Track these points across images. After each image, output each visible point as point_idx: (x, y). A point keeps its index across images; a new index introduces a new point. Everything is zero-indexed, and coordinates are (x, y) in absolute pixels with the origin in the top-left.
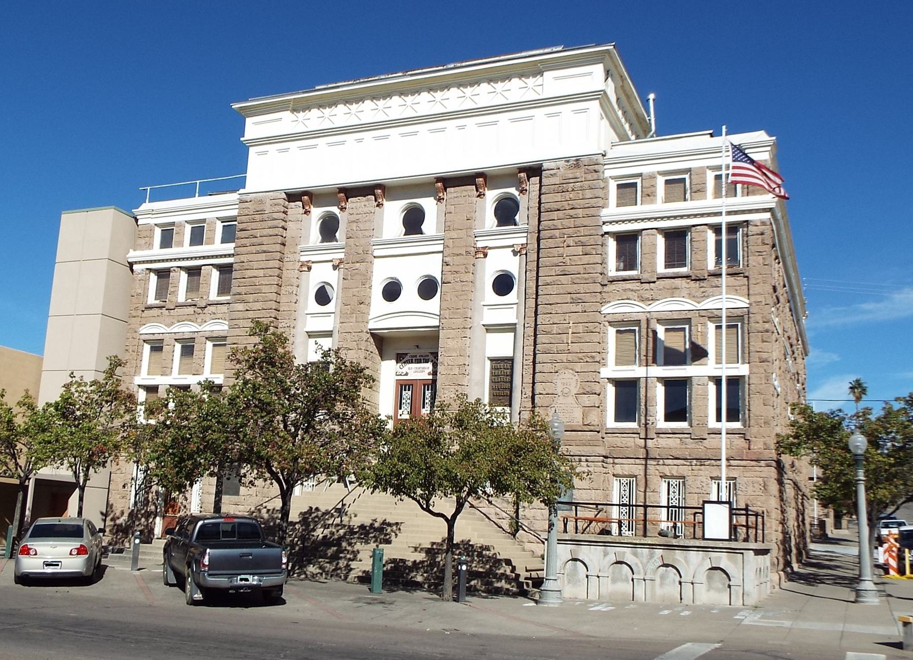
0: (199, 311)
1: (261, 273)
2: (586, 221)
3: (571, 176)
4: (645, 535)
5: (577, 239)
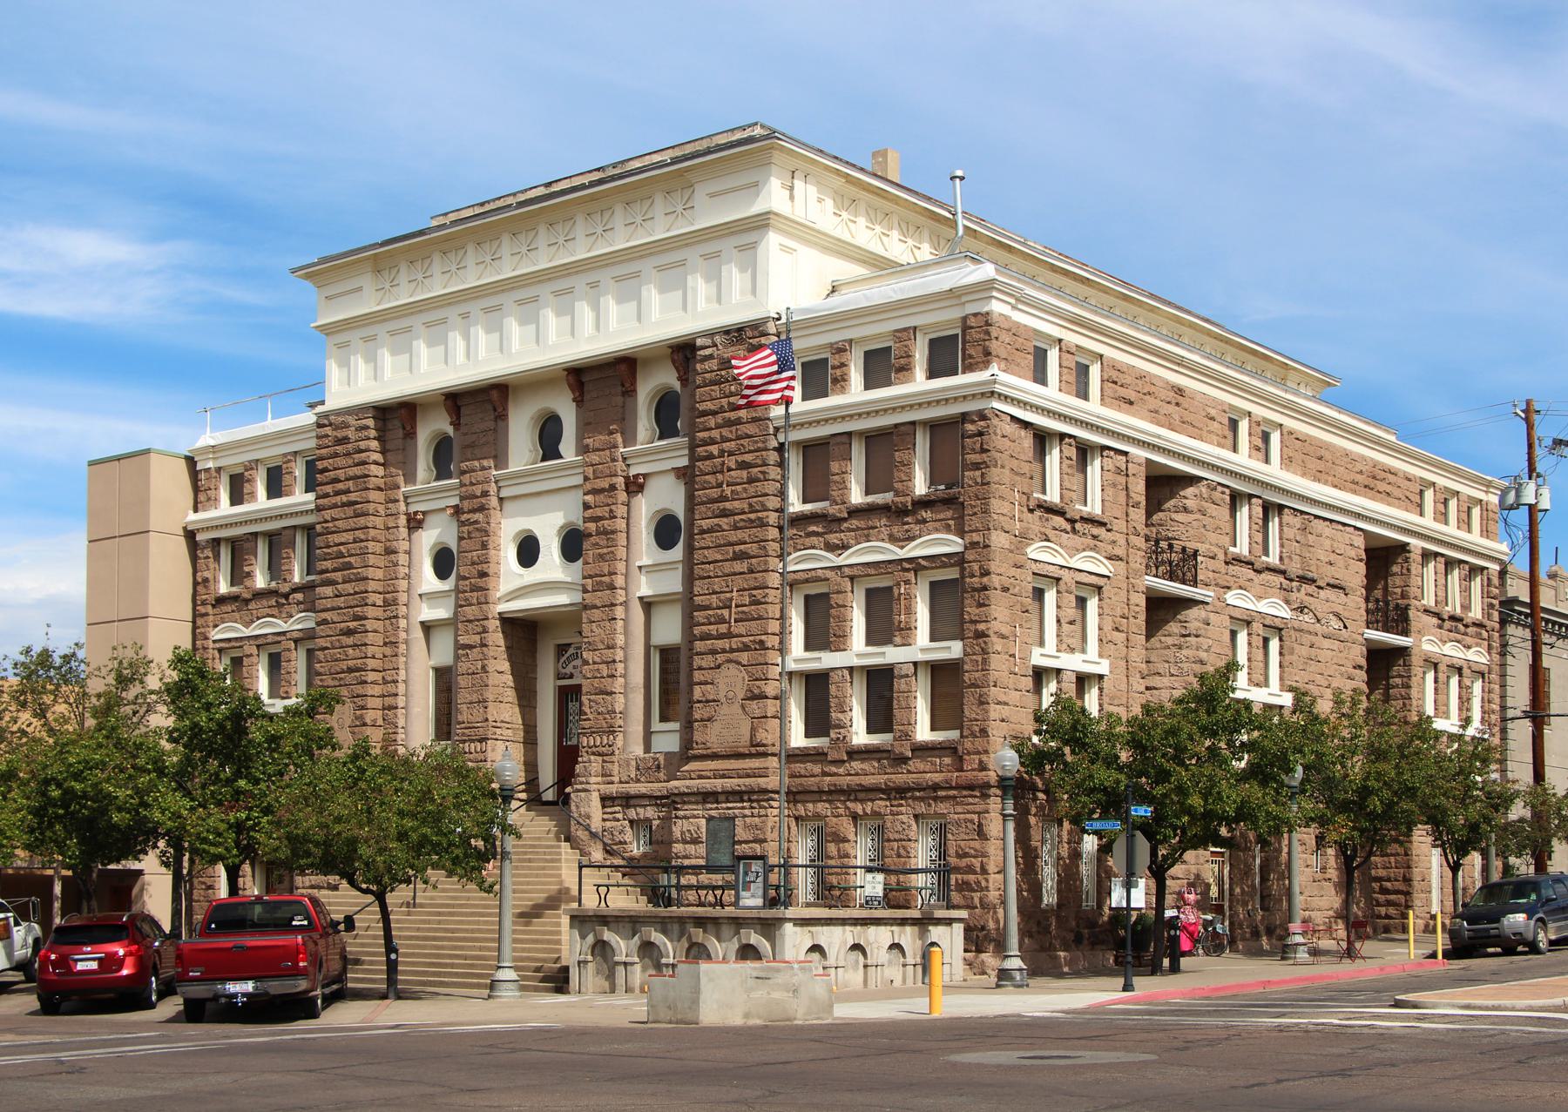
5: (740, 458)
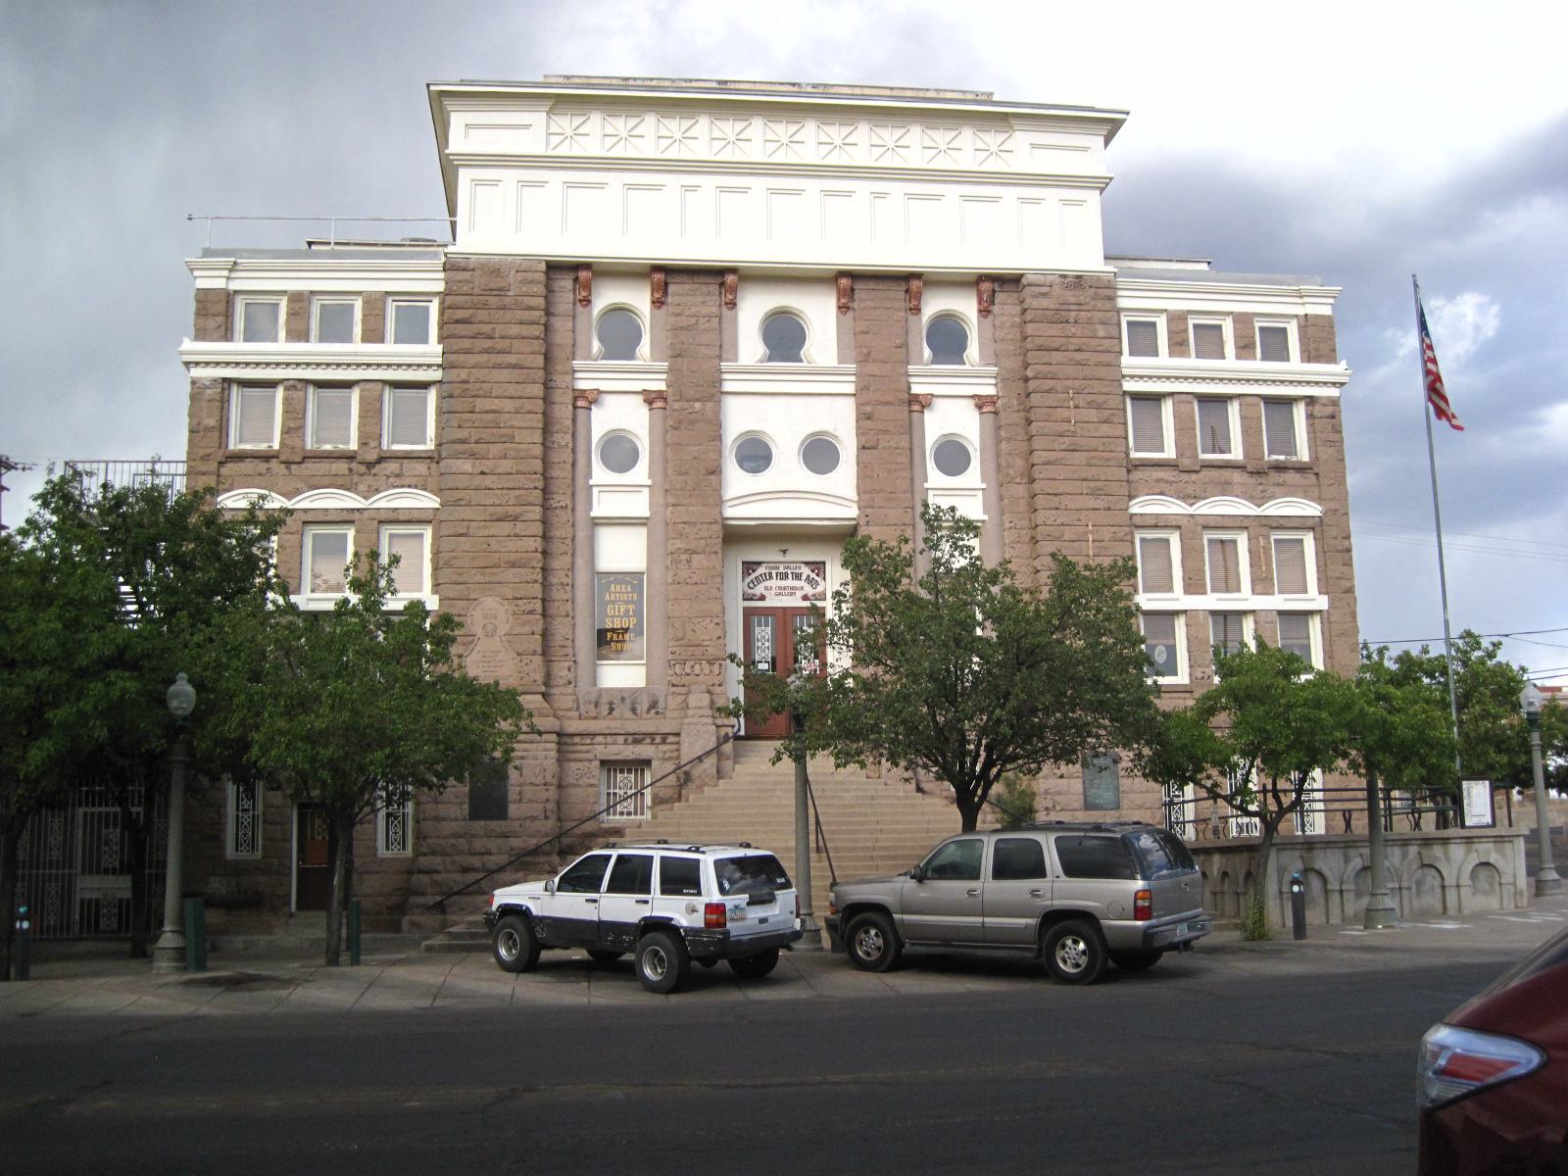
0: (363, 469)
1: (509, 405)
2: (1101, 372)
3: (1073, 300)
4: (1511, 825)
5: (1090, 398)
